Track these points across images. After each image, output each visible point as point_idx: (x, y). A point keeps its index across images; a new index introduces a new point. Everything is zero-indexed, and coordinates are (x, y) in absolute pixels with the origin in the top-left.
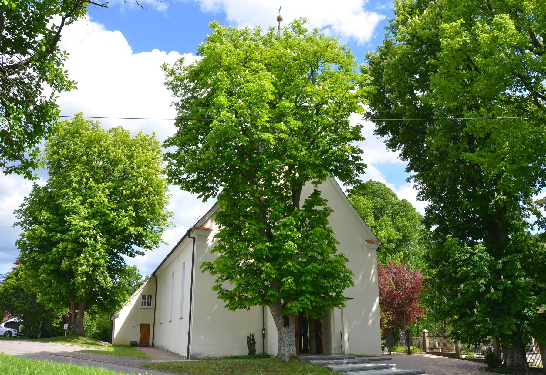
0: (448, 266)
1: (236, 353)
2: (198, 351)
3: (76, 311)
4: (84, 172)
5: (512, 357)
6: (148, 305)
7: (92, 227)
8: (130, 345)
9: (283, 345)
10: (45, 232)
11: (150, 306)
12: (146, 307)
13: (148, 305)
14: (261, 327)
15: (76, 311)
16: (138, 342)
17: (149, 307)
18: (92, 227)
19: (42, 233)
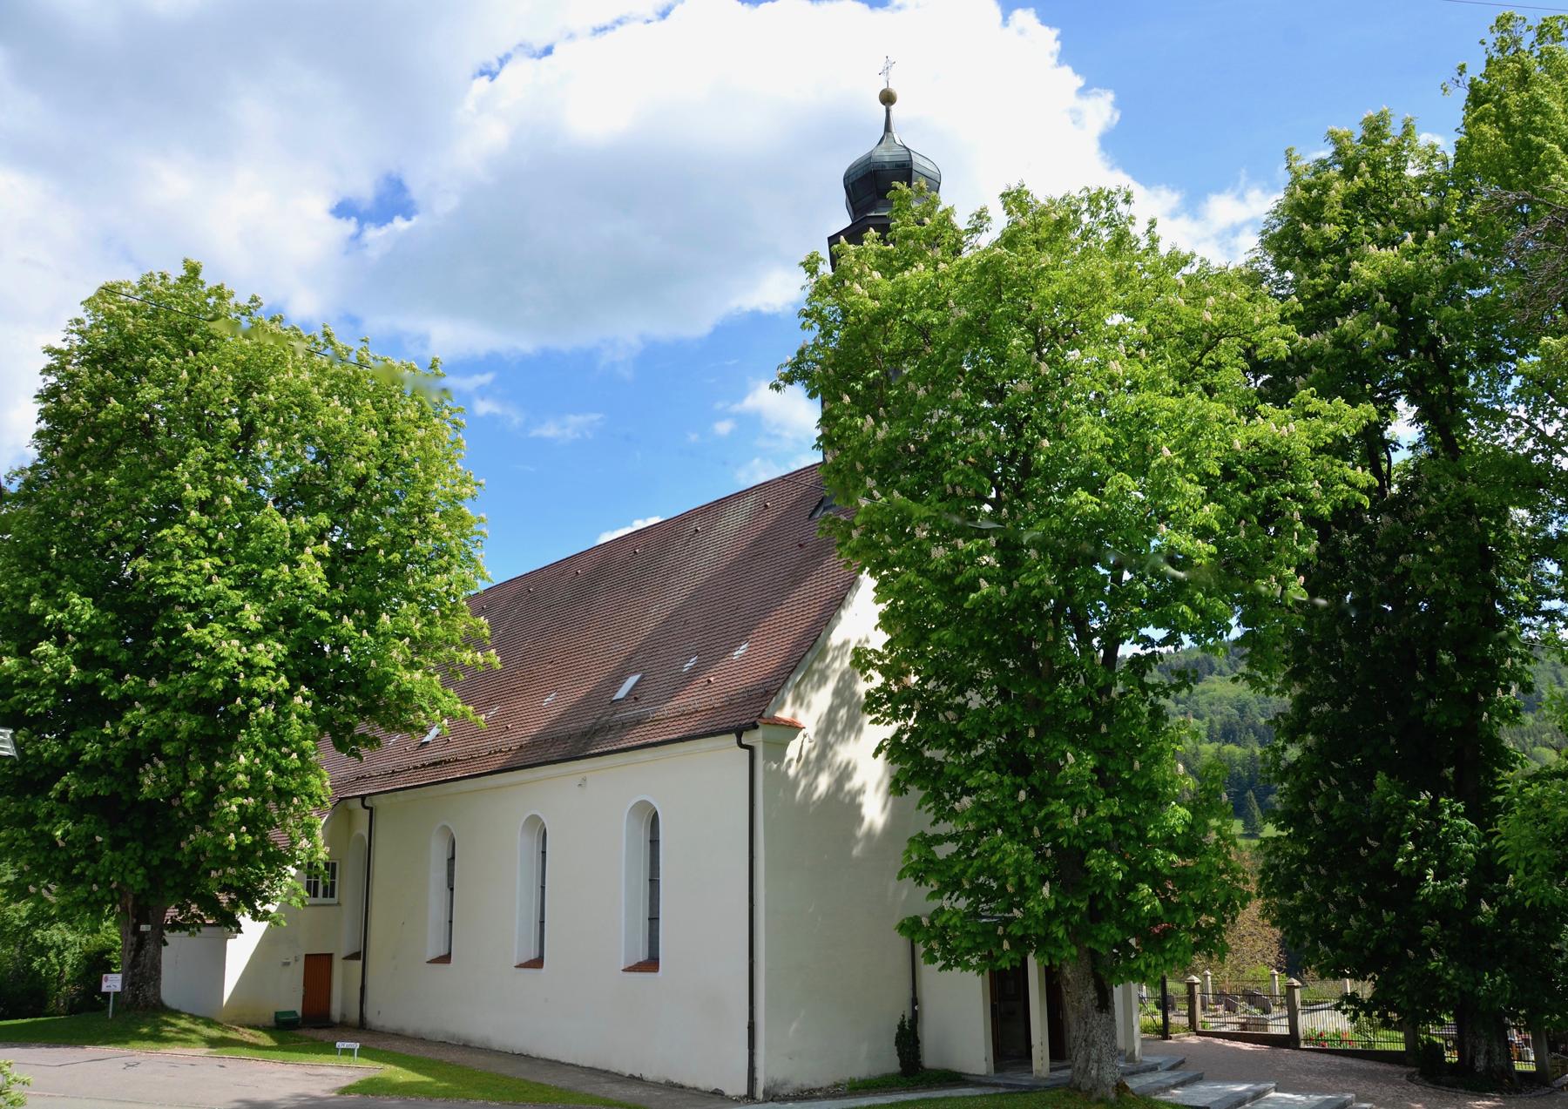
0: (1379, 849)
1: (861, 1069)
2: (779, 1076)
3: (144, 928)
4: (224, 473)
5: (1488, 1052)
6: (325, 895)
7: (273, 664)
8: (270, 1021)
9: (1094, 1056)
10: (74, 669)
11: (332, 896)
12: (320, 899)
13: (325, 895)
14: (908, 994)
15: (144, 928)
16: (300, 1013)
17: (328, 900)
18: (273, 664)
19: (65, 672)
